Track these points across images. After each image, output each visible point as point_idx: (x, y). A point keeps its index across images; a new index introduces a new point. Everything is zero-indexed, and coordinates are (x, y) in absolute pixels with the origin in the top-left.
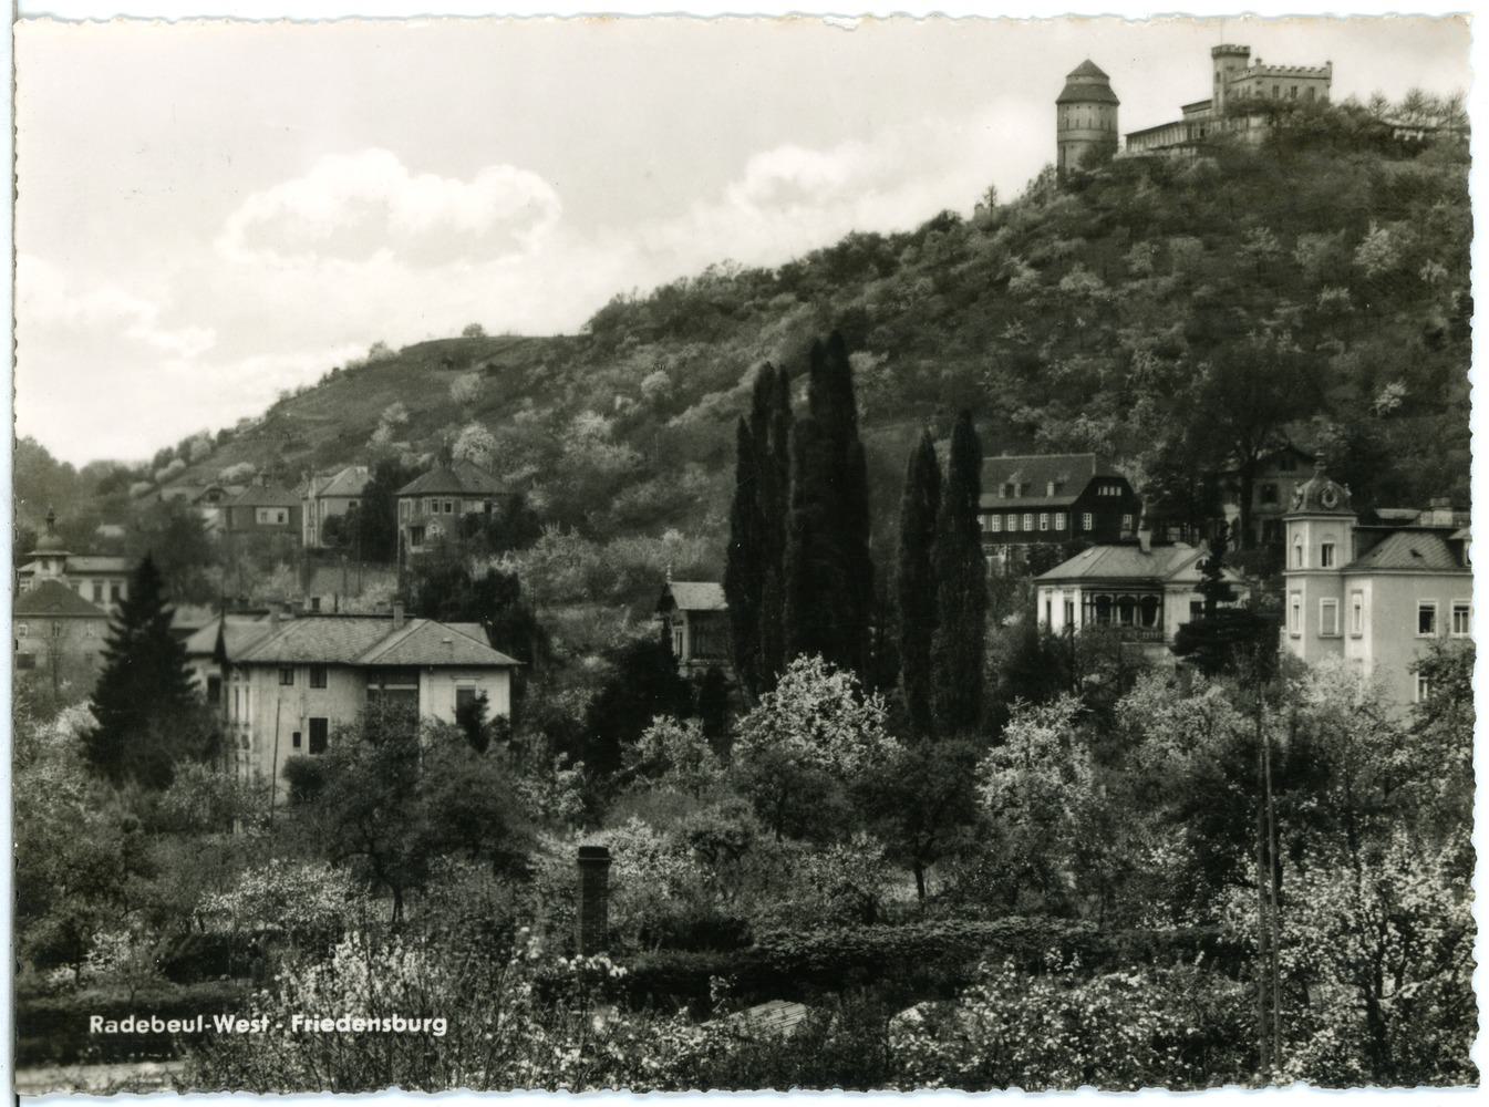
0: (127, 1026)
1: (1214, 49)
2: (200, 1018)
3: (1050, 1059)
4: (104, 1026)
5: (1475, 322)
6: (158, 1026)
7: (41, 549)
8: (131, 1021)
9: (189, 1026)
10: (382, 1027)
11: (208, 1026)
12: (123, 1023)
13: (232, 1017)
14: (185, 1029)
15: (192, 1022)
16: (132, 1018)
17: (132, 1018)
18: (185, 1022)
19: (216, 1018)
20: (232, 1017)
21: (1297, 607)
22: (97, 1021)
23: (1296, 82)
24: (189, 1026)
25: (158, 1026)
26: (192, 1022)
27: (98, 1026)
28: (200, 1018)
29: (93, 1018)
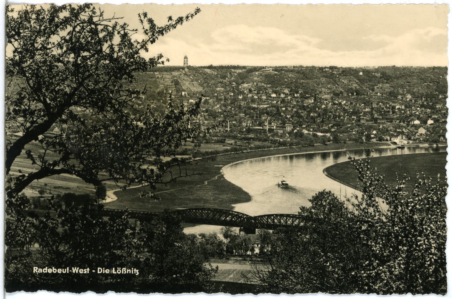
0: (45, 271)
1: (444, 295)
2: (68, 268)
3: (220, 68)
5: (314, 3)
6: (55, 271)
7: (319, 154)
9: (64, 271)
10: (131, 272)
11: (70, 271)
12: (44, 269)
13: (78, 268)
14: (63, 272)
15: (65, 270)
16: (47, 268)
17: (47, 268)
18: (63, 270)
19: (73, 268)
20: (78, 268)
21: (285, 187)
23: (117, 20)
24: (64, 271)
25: (55, 271)
27: (36, 270)
28: (68, 268)
29: (34, 268)
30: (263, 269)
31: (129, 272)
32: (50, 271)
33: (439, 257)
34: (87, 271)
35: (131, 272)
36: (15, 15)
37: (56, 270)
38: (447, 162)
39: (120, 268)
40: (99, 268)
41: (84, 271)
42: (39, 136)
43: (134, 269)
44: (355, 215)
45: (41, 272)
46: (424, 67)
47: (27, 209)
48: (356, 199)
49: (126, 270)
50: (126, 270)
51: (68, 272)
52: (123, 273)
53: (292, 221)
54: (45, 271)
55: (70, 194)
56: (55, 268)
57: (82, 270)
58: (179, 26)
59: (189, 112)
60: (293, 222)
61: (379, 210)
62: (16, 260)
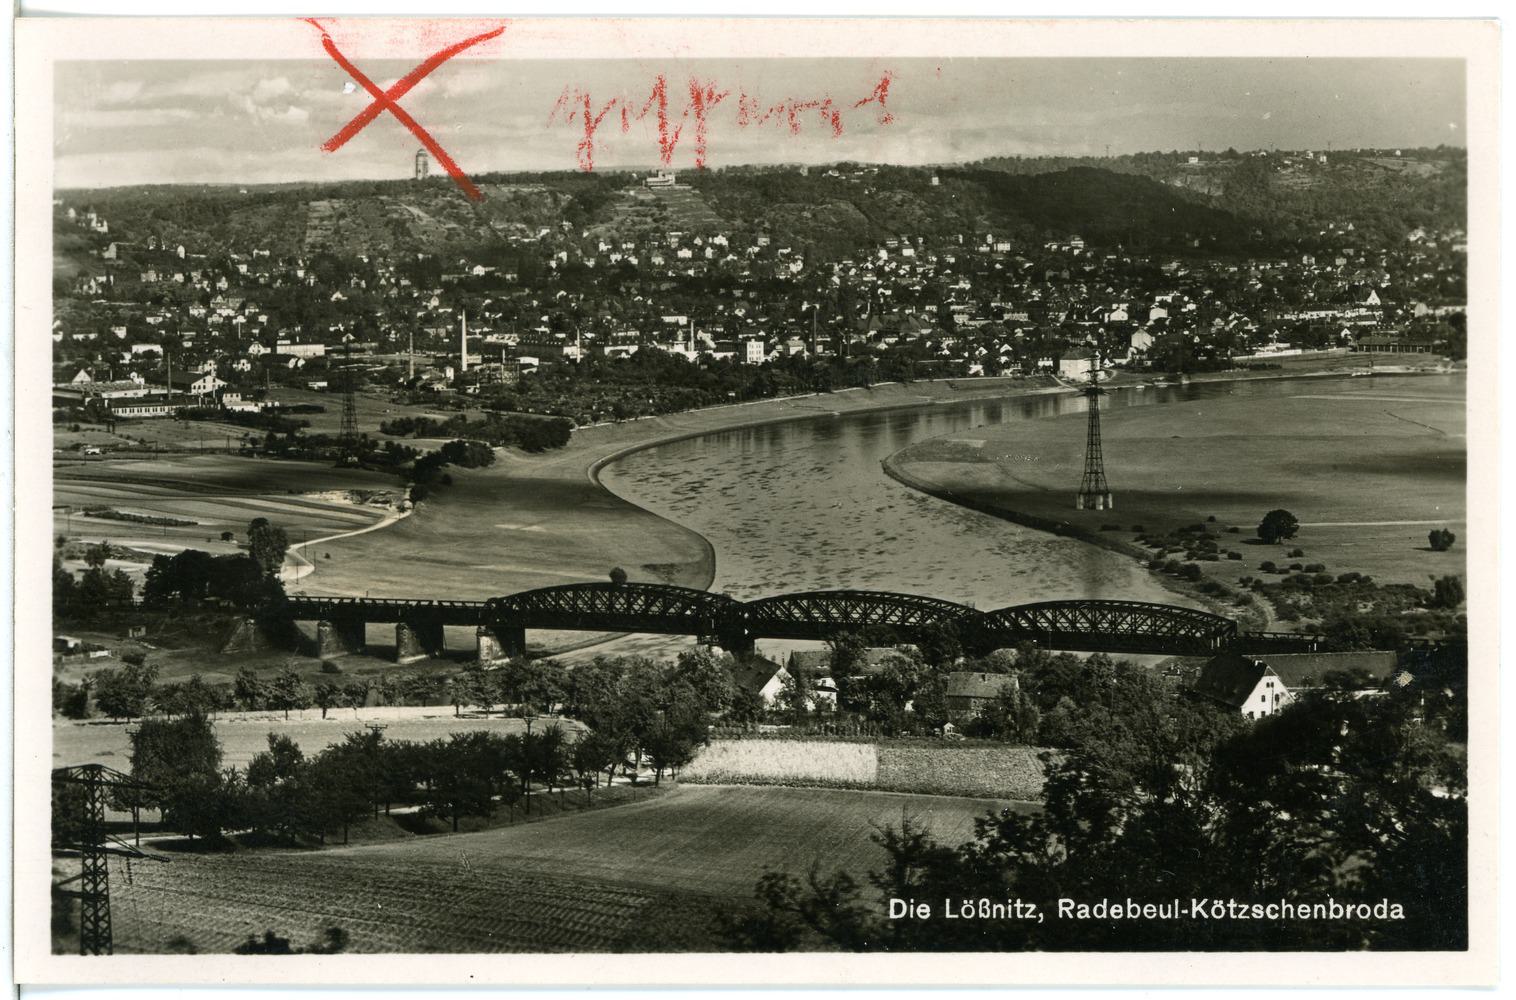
9: (1320, 910)
10: (1006, 912)
11: (1185, 912)
25: (1134, 911)
32: (1116, 911)
35: (1006, 912)
39: (1221, 902)
40: (893, 902)
42: (367, 624)
43: (1014, 902)
44: (327, 213)
45: (1087, 916)
47: (1285, 816)
48: (833, 121)
49: (991, 907)
50: (991, 907)
52: (981, 915)
53: (646, 602)
54: (1380, 912)
55: (77, 718)
58: (598, 125)
60: (630, 605)
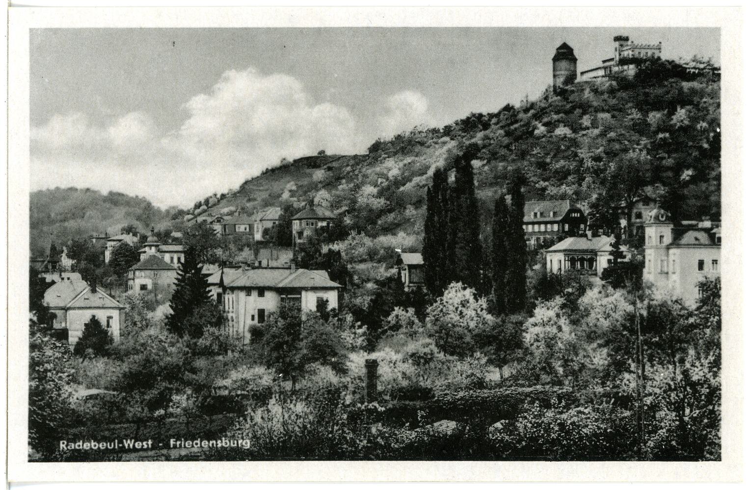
4: (67, 446)
8: (81, 443)
9: (110, 446)
11: (121, 445)
15: (112, 444)
16: (199, 439)
19: (124, 441)
22: (63, 443)
24: (110, 446)
25: (95, 446)
26: (112, 444)
28: (116, 441)
30: (338, 211)
31: (213, 444)
33: (561, 449)
34: (147, 444)
36: (33, 388)
37: (96, 443)
38: (86, 325)
41: (143, 446)
46: (721, 365)
51: (116, 447)
54: (79, 446)
56: (94, 442)
57: (140, 443)
59: (647, 379)
61: (501, 323)
62: (596, 419)
